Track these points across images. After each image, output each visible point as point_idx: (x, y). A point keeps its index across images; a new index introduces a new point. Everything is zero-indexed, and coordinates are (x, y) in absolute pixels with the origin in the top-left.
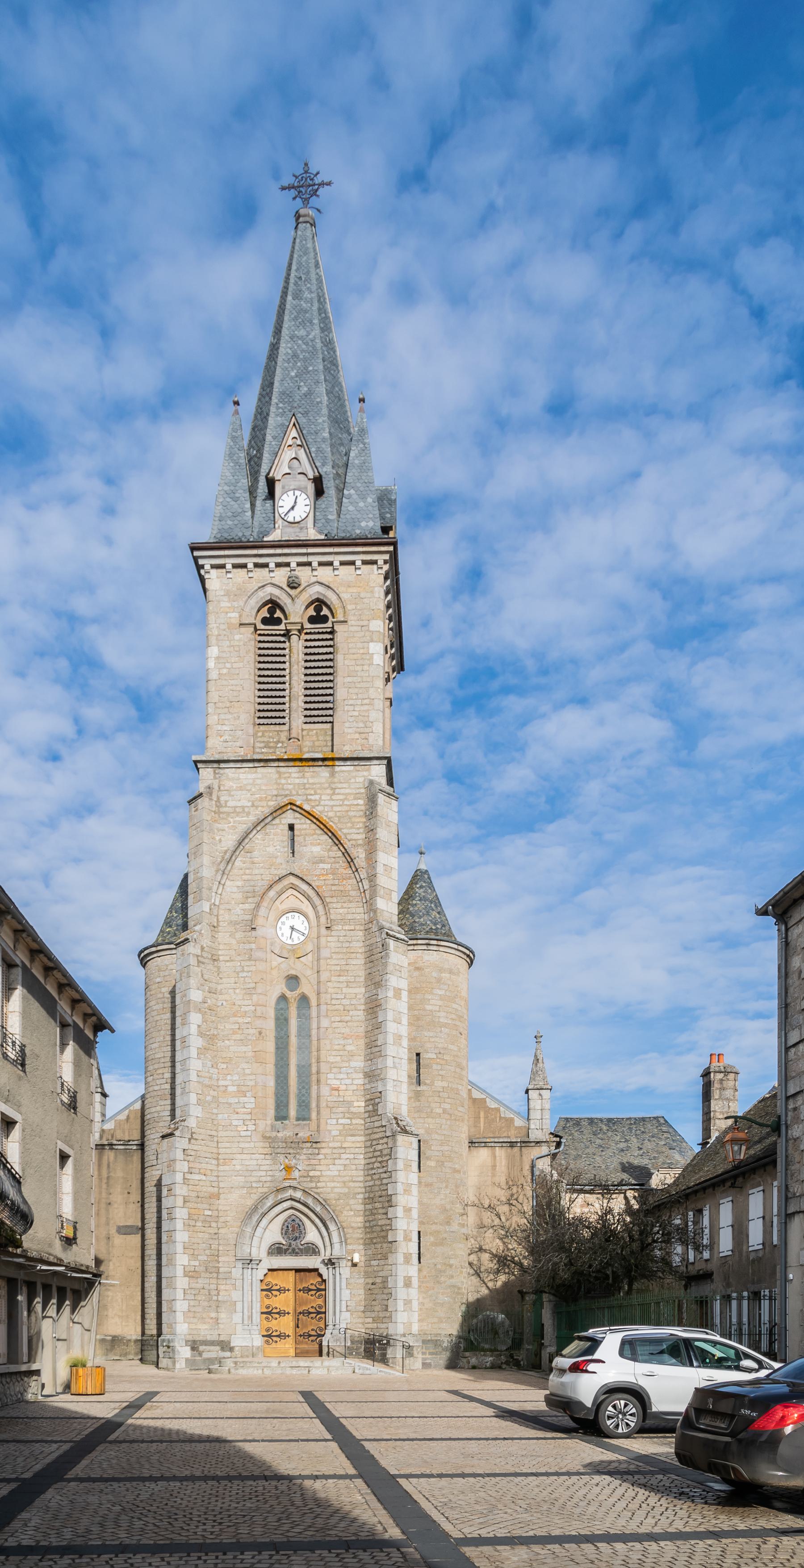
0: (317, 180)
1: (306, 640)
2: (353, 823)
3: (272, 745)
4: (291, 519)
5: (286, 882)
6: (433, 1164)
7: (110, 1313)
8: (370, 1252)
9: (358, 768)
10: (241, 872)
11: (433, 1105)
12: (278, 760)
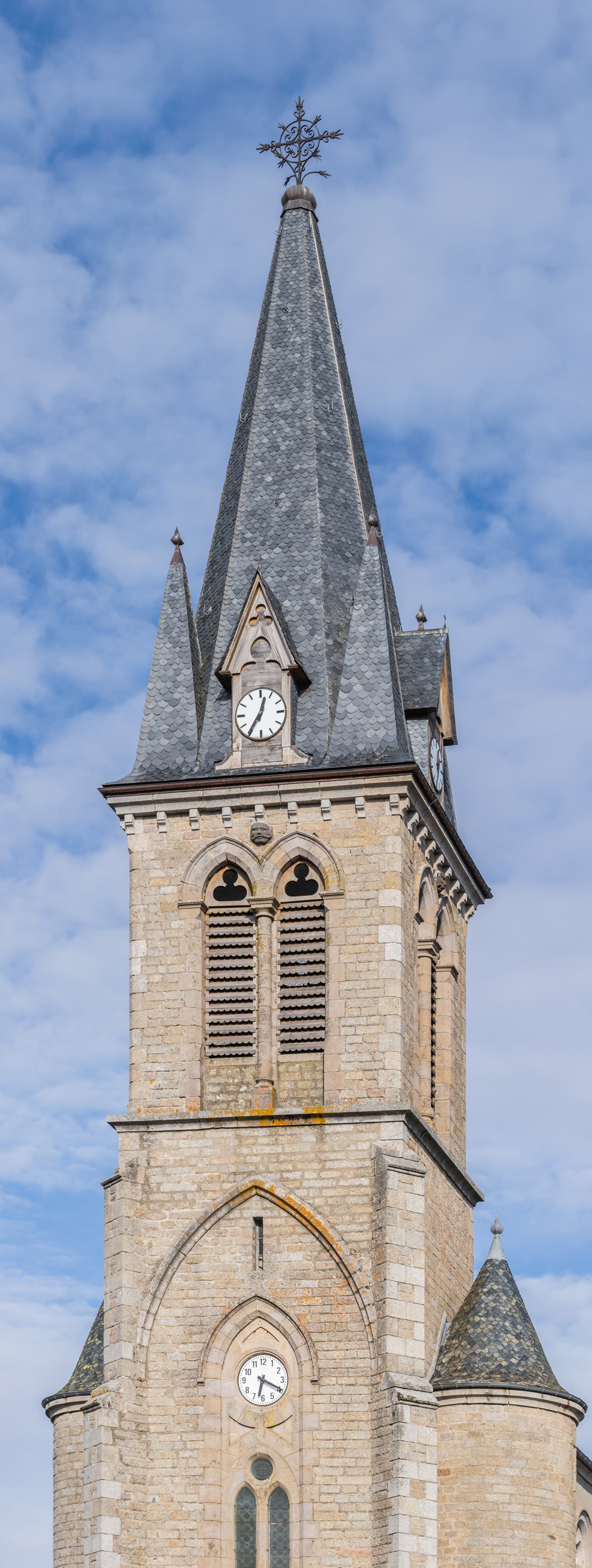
1: (283, 921)
2: (352, 1215)
3: (231, 1088)
4: (255, 734)
5: (249, 1309)
9: (361, 1127)
10: (182, 1294)
12: (237, 1119)
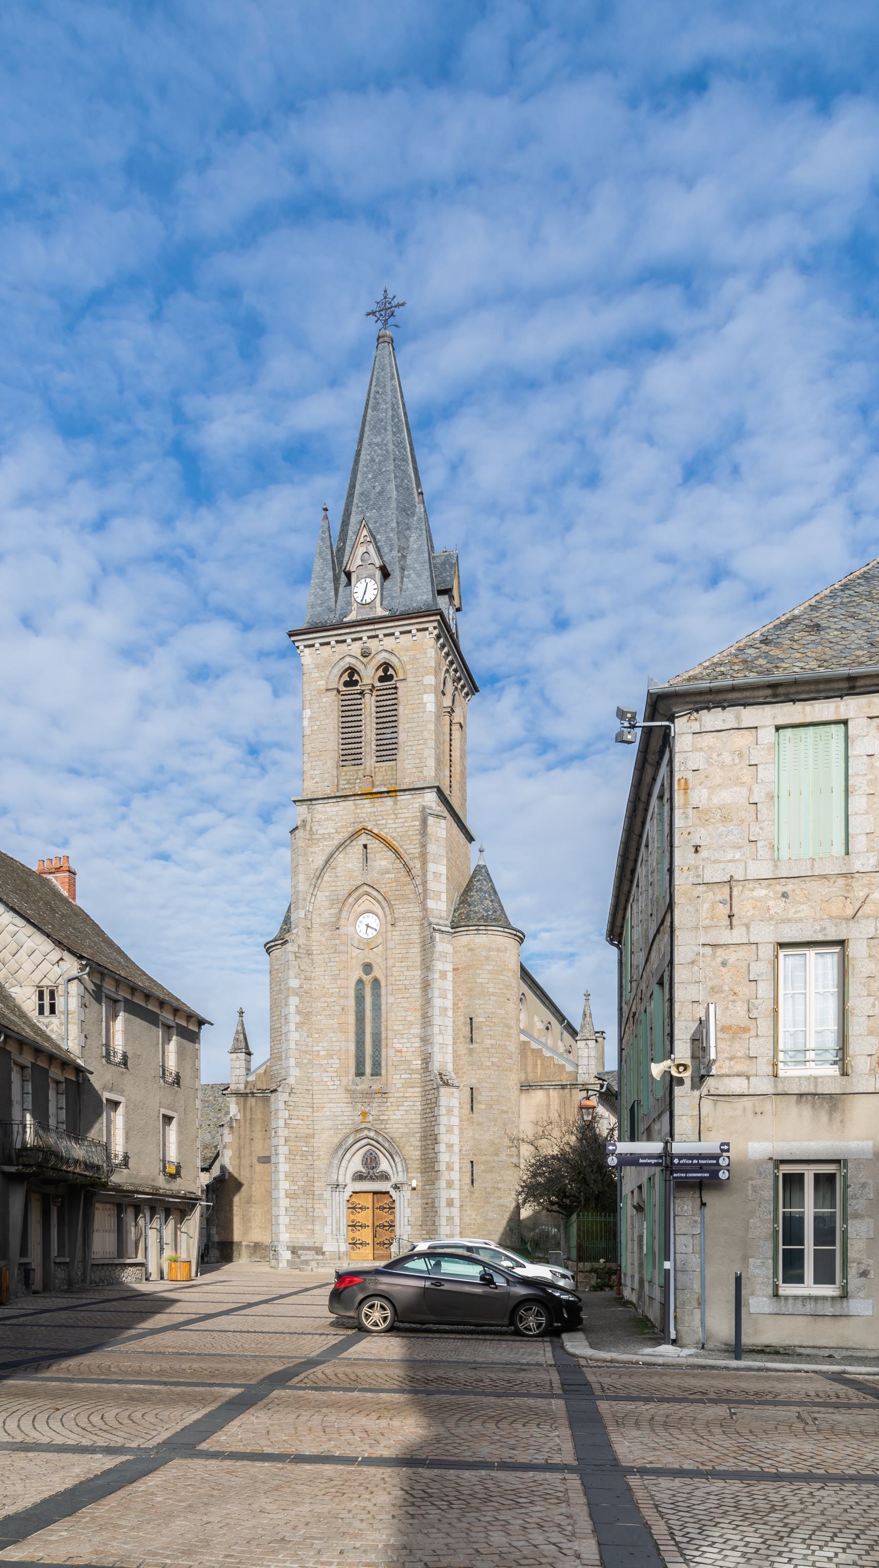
0: (394, 303)
2: (411, 840)
5: (361, 890)
6: (483, 1107)
7: (254, 1224)
8: (424, 1179)
11: (483, 1059)
12: (355, 795)
